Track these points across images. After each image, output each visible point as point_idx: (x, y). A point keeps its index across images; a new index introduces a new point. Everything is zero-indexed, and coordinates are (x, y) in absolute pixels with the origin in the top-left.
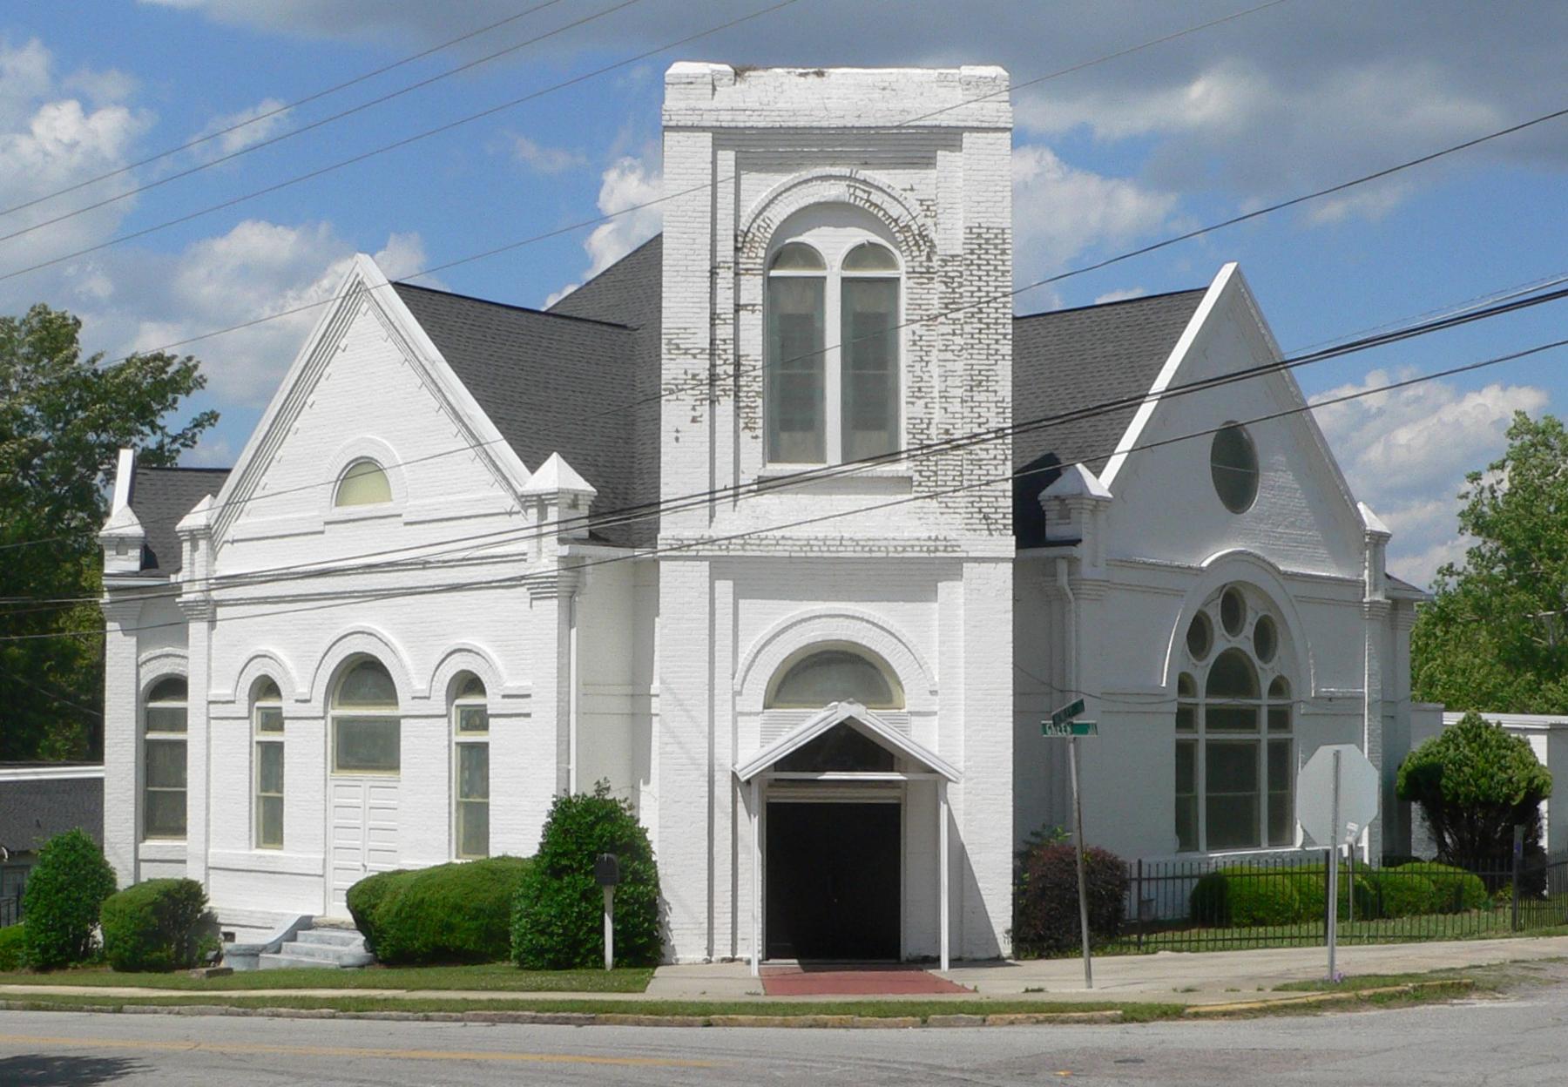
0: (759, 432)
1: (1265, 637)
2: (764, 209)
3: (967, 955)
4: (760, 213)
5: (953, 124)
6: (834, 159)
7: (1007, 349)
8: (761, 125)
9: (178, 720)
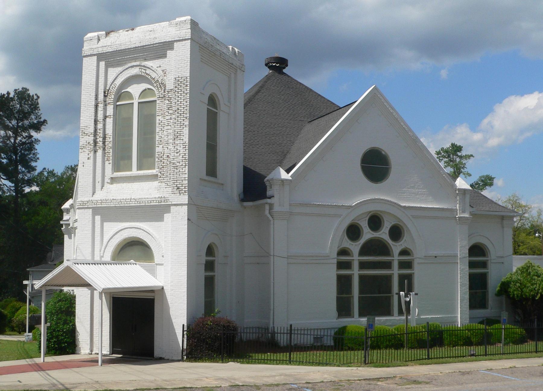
0: (111, 161)
1: (396, 233)
2: (114, 81)
3: (170, 358)
4: (113, 82)
5: (170, 40)
6: (135, 59)
7: (187, 123)
8: (110, 51)
9: (484, 265)
